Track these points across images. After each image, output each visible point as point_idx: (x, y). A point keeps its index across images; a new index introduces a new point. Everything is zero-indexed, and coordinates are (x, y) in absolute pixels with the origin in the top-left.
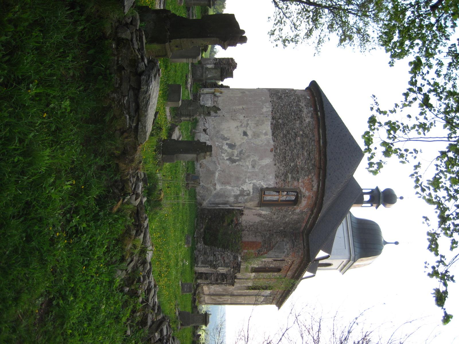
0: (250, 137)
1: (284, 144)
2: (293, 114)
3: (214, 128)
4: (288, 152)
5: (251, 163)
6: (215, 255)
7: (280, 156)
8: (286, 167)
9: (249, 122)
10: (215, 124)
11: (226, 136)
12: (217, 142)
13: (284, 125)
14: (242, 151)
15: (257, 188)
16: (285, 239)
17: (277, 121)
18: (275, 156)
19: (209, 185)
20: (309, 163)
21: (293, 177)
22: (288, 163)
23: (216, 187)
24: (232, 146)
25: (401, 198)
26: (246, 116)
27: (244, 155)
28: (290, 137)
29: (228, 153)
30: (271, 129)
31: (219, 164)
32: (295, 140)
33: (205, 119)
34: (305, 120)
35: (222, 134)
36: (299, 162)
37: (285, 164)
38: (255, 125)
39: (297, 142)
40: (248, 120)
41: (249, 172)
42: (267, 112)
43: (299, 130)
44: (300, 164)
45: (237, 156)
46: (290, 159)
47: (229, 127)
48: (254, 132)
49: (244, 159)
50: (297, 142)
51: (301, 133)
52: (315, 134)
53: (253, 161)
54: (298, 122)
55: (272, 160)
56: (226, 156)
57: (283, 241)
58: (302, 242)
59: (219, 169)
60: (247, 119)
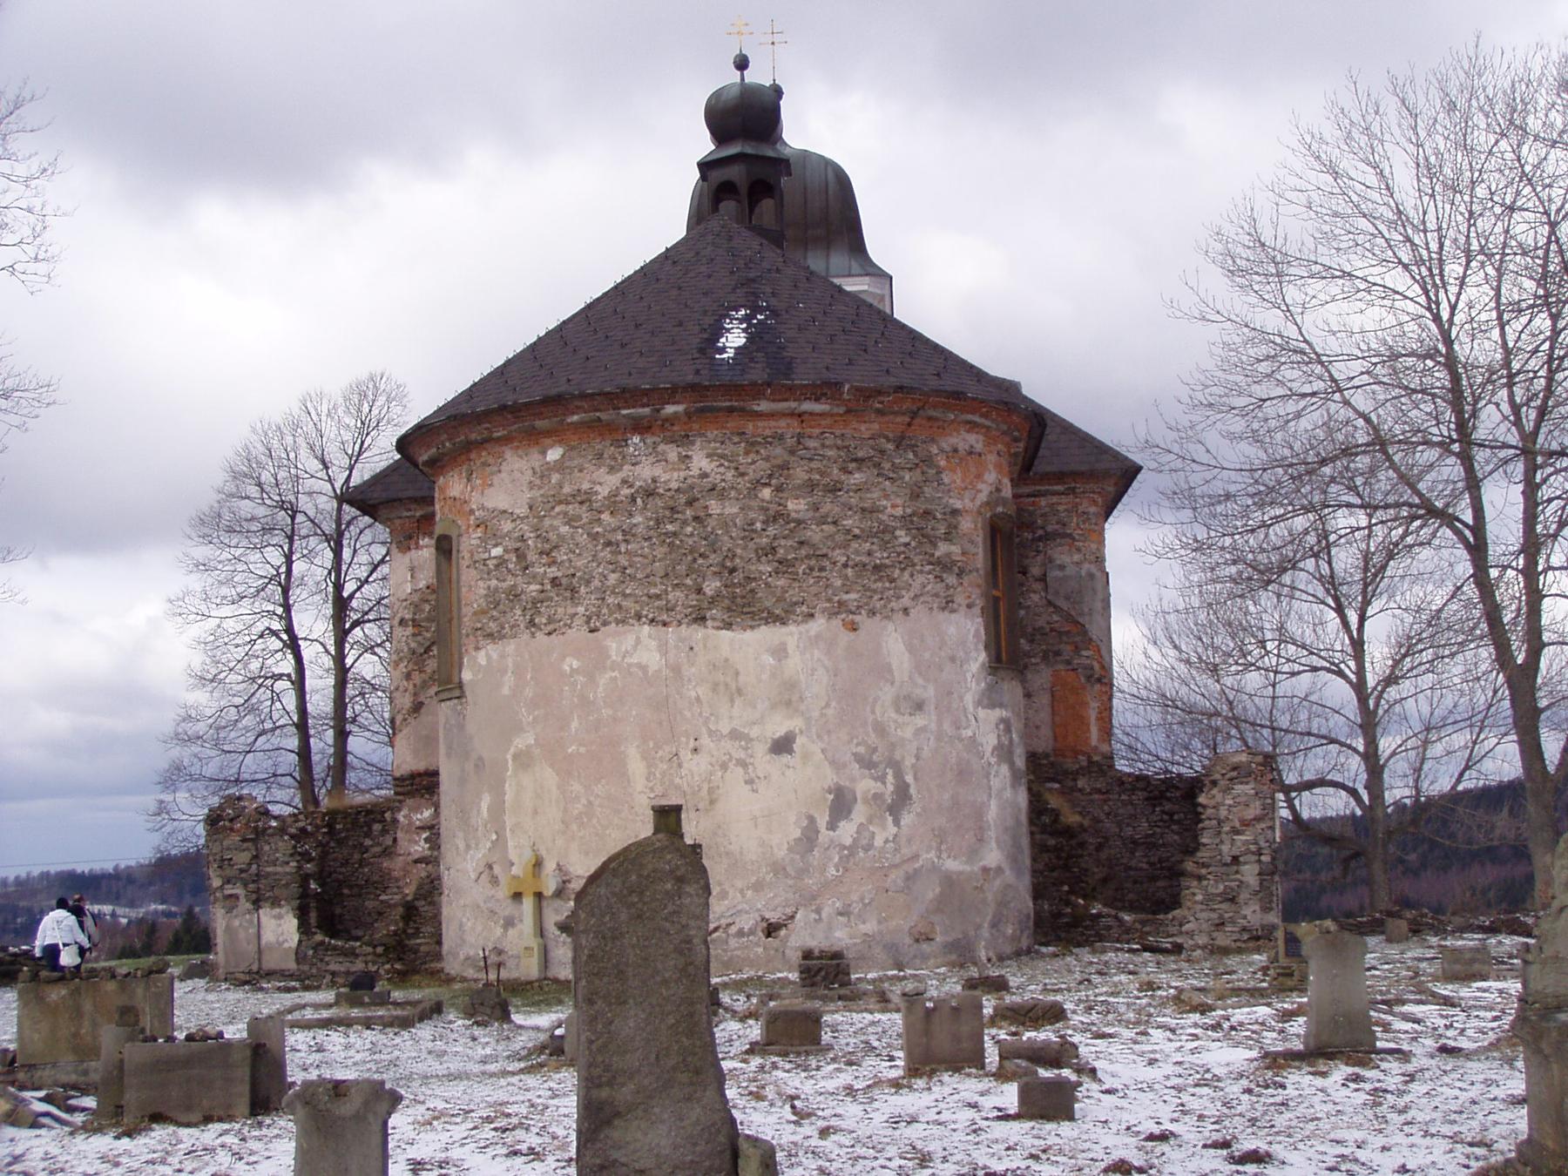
0: (795, 724)
1: (822, 569)
2: (670, 527)
3: (758, 887)
4: (857, 552)
5: (907, 718)
6: (1235, 859)
7: (875, 591)
8: (914, 565)
9: (725, 731)
10: (739, 884)
11: (797, 833)
12: (823, 870)
13: (732, 571)
14: (858, 758)
15: (991, 688)
16: (1035, 571)
17: (713, 601)
18: (872, 613)
19: (990, 896)
20: (893, 464)
21: (948, 537)
22: (899, 554)
23: (993, 865)
24: (841, 804)
25: (742, 64)
26: (692, 744)
27: (875, 750)
28: (790, 543)
29: (870, 821)
30: (752, 627)
31: (916, 857)
32: (799, 522)
33: (716, 929)
34: (704, 475)
35: (790, 850)
36: (893, 506)
37: (903, 570)
38: (738, 702)
39: (811, 514)
40: (711, 733)
41: (940, 723)
42: (663, 649)
43: (754, 504)
44: (899, 501)
45: (882, 779)
46: (884, 545)
47: (755, 818)
48: (774, 707)
49: (892, 747)
50: (811, 514)
51: (766, 493)
52: (768, 432)
53: (898, 711)
54: (715, 507)
55: (891, 627)
56: (884, 827)
57: (1043, 579)
58: (1043, 502)
59: (932, 855)
60: (705, 741)
